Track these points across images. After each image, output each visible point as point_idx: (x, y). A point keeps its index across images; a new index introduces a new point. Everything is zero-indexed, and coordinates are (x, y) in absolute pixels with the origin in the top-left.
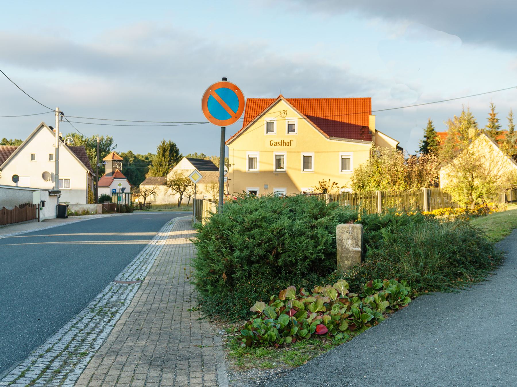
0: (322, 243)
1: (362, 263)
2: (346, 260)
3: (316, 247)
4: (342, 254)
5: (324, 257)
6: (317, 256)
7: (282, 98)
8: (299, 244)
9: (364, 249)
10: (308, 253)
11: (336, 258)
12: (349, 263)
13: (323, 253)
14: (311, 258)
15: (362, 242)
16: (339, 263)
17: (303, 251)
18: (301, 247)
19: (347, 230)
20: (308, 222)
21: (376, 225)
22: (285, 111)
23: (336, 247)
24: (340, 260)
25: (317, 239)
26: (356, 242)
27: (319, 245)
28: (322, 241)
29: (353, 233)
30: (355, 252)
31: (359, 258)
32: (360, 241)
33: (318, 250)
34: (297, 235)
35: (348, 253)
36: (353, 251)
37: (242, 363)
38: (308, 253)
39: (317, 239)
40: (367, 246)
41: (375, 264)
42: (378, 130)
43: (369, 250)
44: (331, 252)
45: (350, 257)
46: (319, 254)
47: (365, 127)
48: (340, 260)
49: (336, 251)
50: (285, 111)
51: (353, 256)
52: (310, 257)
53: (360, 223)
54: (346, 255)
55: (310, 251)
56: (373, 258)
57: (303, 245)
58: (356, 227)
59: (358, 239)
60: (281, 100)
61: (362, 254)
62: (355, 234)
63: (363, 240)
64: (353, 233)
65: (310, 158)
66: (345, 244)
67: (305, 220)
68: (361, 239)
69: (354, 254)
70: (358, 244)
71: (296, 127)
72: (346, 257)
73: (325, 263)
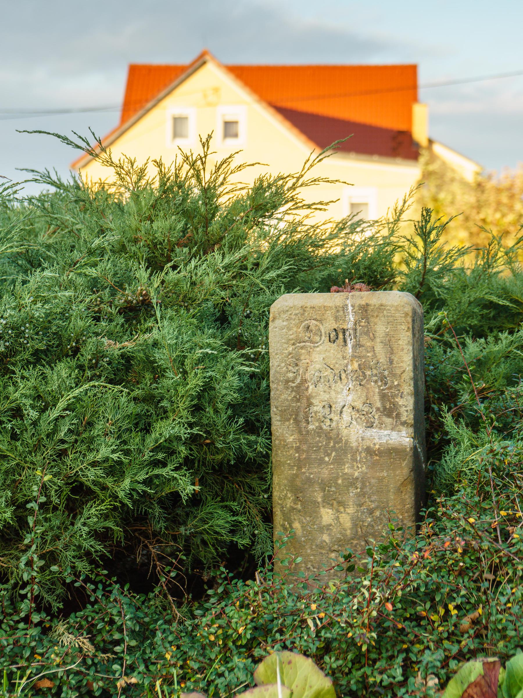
0: (183, 405)
1: (419, 519)
2: (328, 501)
3: (147, 429)
4: (299, 464)
5: (190, 488)
6: (148, 482)
7: (207, 58)
8: (34, 414)
9: (429, 435)
10: (94, 464)
11: (268, 490)
12: (346, 521)
13: (188, 462)
14: (115, 497)
15: (416, 393)
16: (286, 517)
17: (63, 453)
18: (45, 427)
19: (330, 325)
20: (110, 281)
21: (492, 305)
22: (216, 90)
23: (269, 424)
24: (289, 503)
25: (155, 380)
26: (383, 397)
27: (164, 414)
28: (181, 390)
29: (365, 341)
30: (380, 453)
31: (399, 491)
32: (408, 388)
33: (156, 449)
34: (26, 356)
35: (339, 461)
36: (369, 451)
37: (164, 631)
38: (94, 464)
39: (155, 380)
40: (448, 420)
41: (506, 536)
42: (434, 137)
43: (458, 444)
44: (241, 457)
45: (352, 482)
46: (165, 472)
47: (401, 133)
48: (289, 503)
49: (269, 447)
50: (216, 90)
51: (364, 480)
52: (104, 488)
53: (409, 291)
54: (325, 473)
55: (104, 452)
56: (487, 496)
57: (54, 414)
58: (381, 307)
59: (393, 375)
60: (204, 63)
61: (416, 469)
62: (379, 348)
63: (422, 387)
64: (365, 341)
65: (234, 125)
66: (317, 407)
67: (93, 272)
68: (415, 380)
69: (373, 466)
70: (395, 405)
71: (242, 129)
72: (324, 486)
73: (204, 521)
